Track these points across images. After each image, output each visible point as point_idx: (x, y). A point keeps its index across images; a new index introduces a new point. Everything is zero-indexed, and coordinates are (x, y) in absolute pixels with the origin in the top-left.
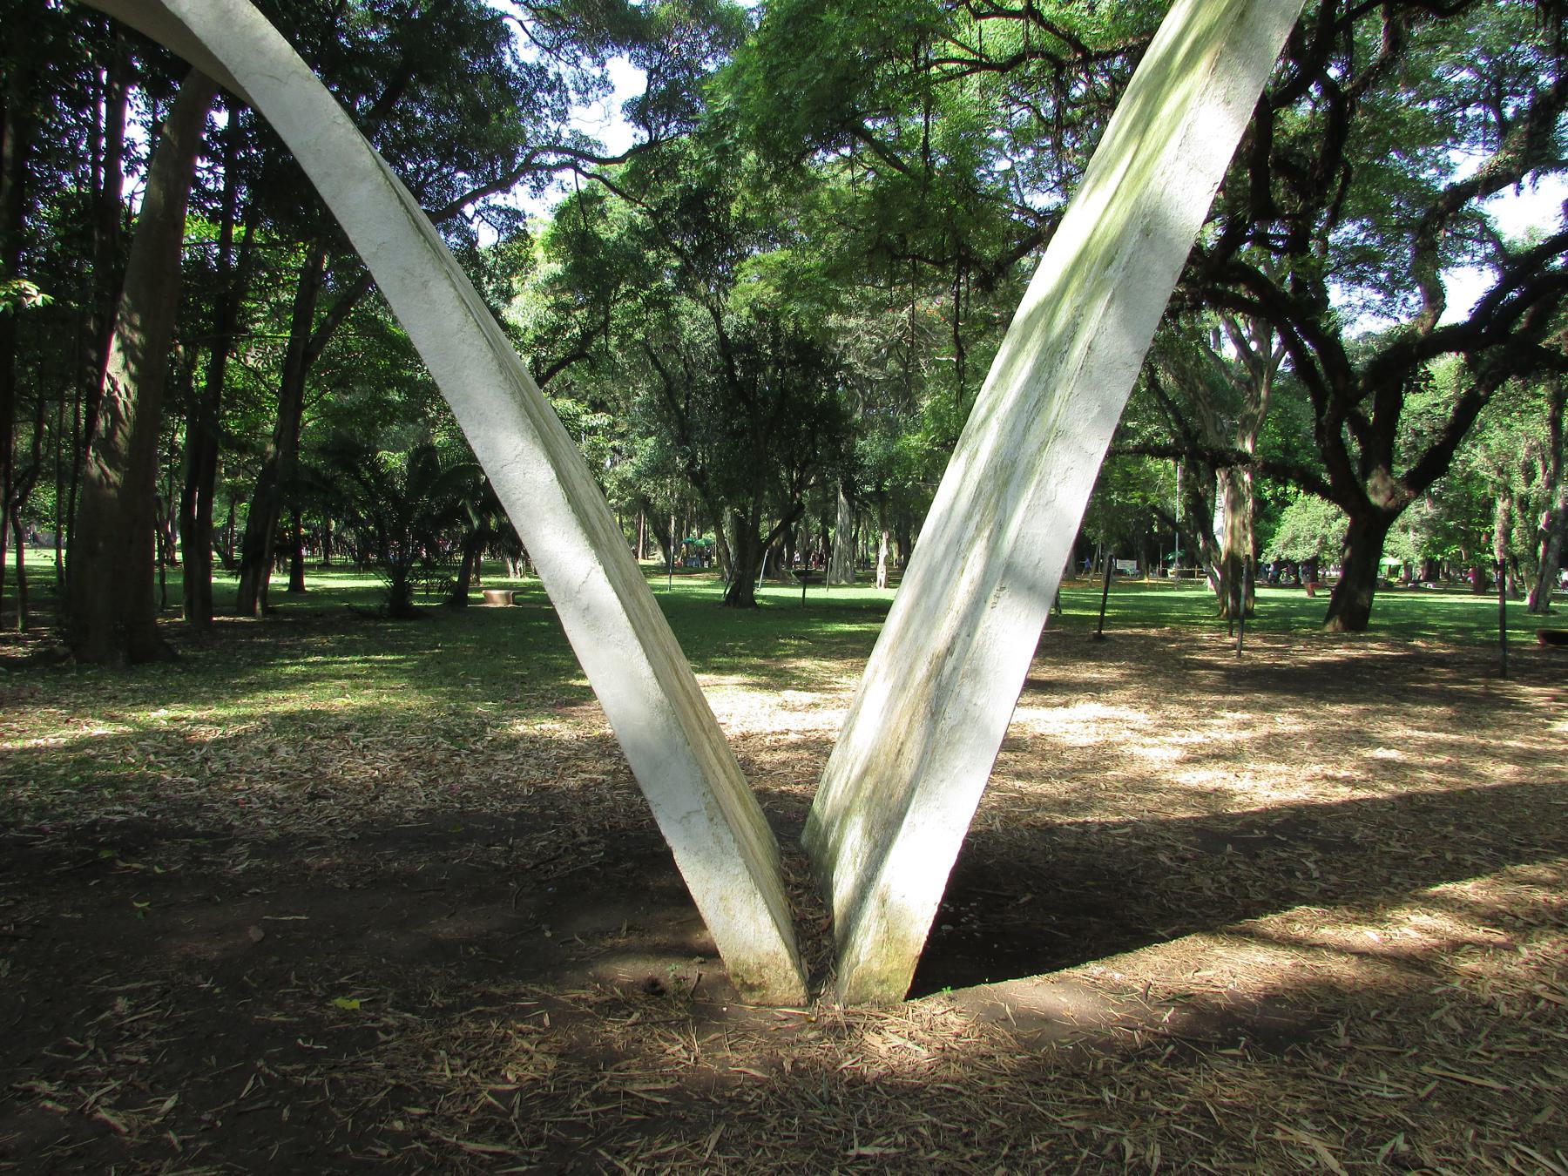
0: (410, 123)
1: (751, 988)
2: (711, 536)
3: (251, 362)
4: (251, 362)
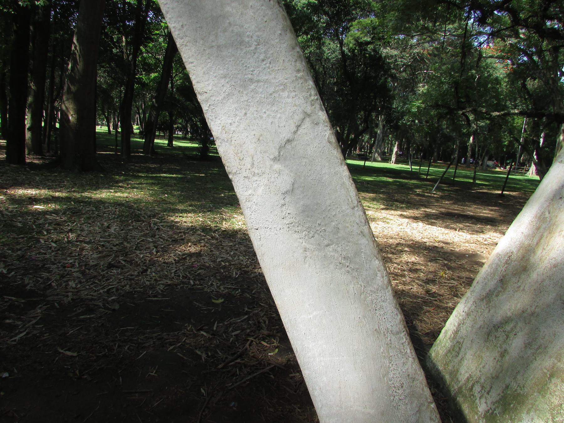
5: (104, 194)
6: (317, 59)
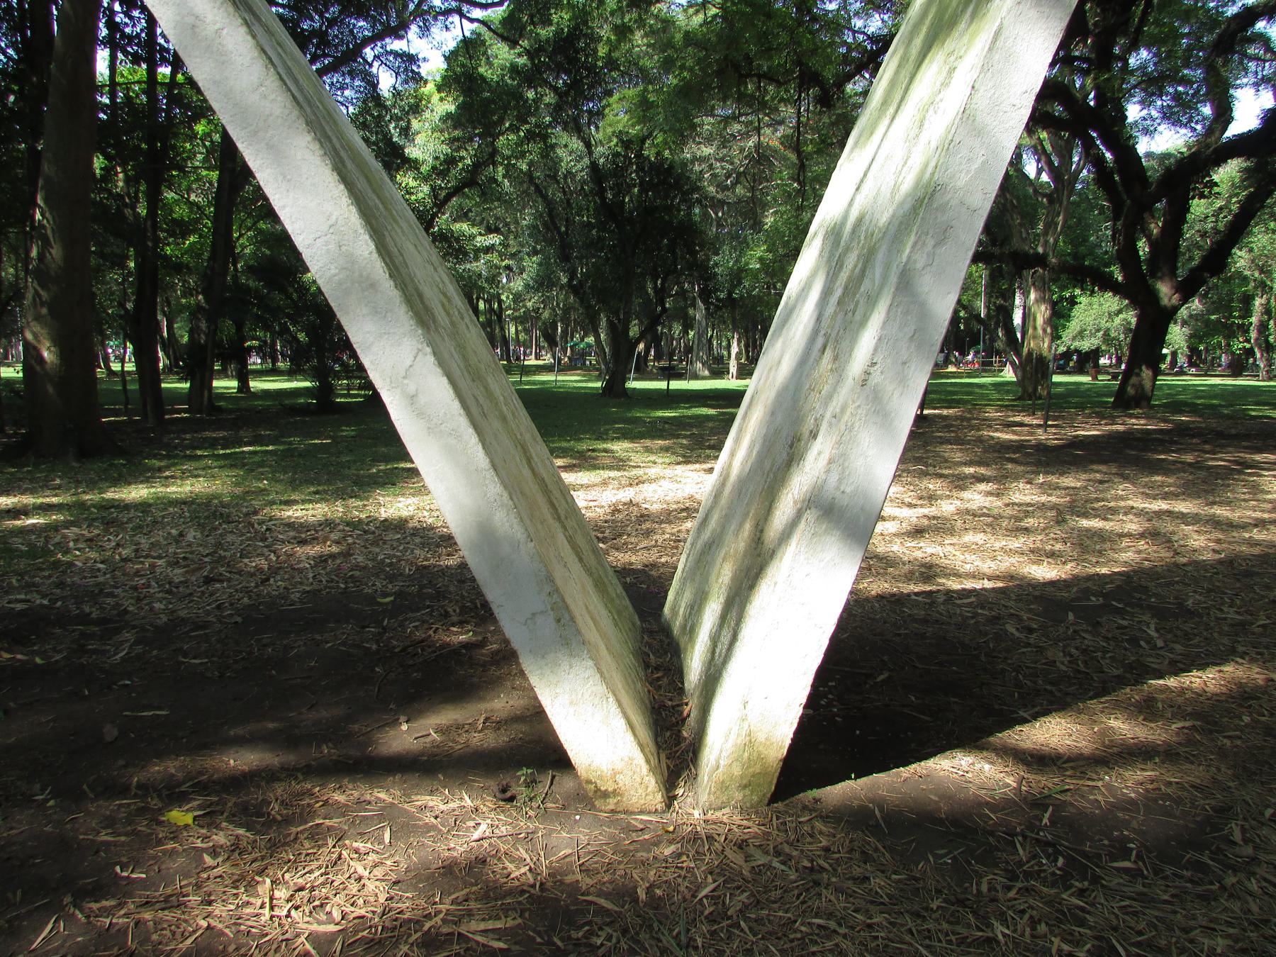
1: (605, 795)
2: (591, 340)
5: (137, 493)
6: (548, 176)
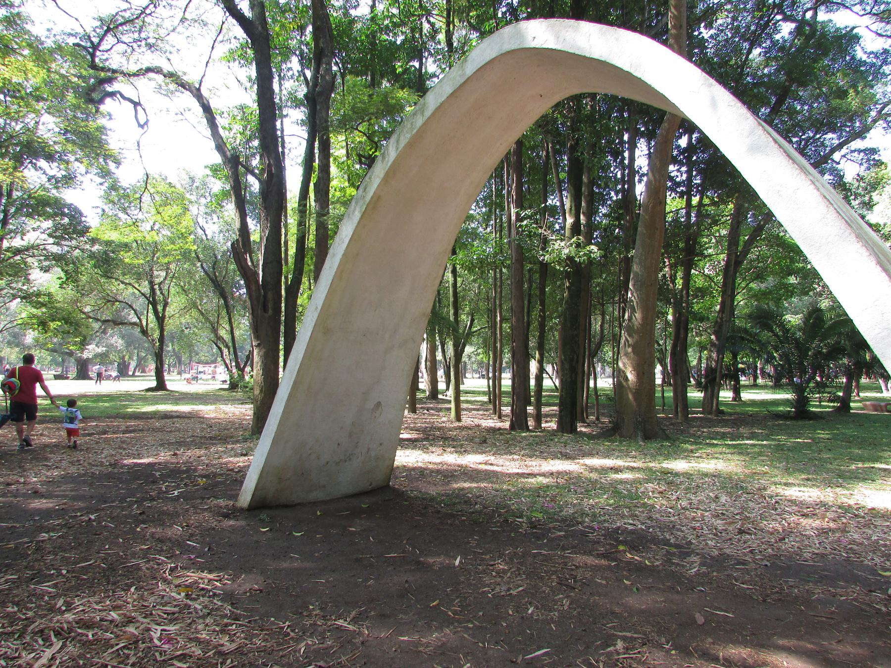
0: (792, 113)
3: (706, 271)
4: (706, 271)
5: (679, 465)
